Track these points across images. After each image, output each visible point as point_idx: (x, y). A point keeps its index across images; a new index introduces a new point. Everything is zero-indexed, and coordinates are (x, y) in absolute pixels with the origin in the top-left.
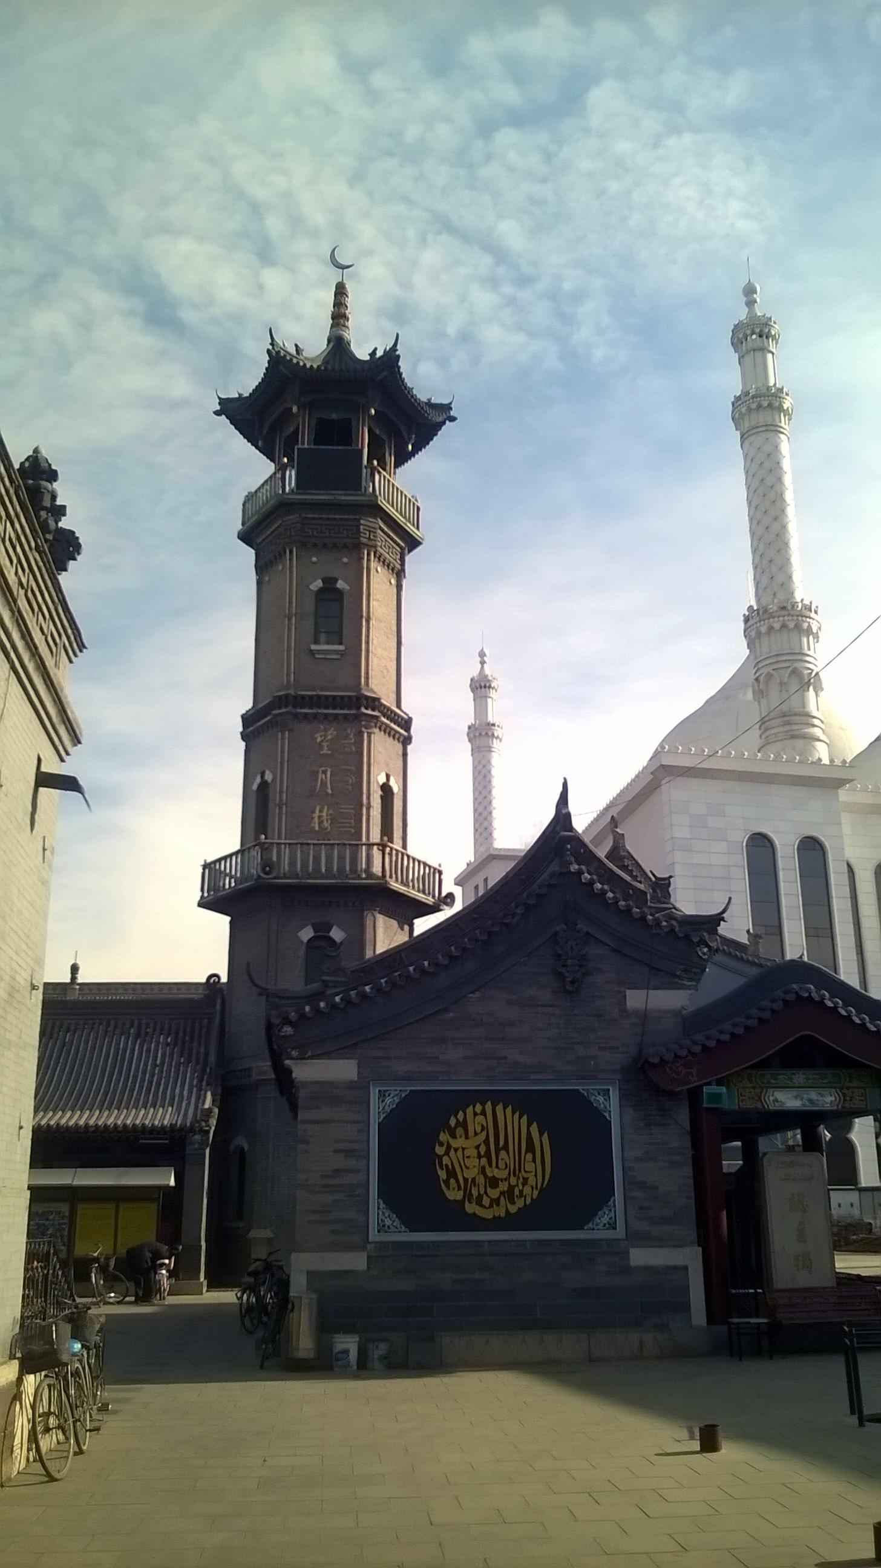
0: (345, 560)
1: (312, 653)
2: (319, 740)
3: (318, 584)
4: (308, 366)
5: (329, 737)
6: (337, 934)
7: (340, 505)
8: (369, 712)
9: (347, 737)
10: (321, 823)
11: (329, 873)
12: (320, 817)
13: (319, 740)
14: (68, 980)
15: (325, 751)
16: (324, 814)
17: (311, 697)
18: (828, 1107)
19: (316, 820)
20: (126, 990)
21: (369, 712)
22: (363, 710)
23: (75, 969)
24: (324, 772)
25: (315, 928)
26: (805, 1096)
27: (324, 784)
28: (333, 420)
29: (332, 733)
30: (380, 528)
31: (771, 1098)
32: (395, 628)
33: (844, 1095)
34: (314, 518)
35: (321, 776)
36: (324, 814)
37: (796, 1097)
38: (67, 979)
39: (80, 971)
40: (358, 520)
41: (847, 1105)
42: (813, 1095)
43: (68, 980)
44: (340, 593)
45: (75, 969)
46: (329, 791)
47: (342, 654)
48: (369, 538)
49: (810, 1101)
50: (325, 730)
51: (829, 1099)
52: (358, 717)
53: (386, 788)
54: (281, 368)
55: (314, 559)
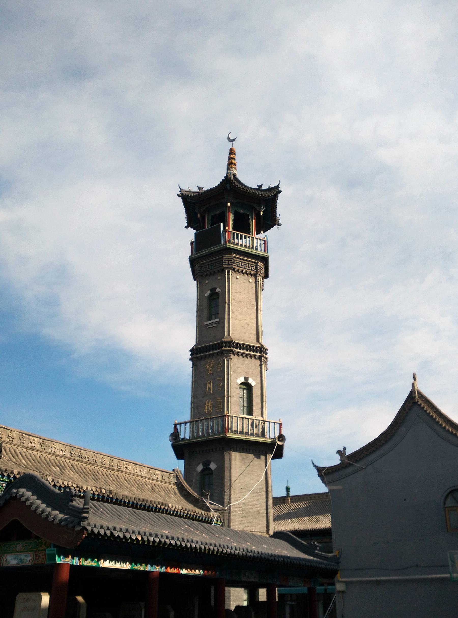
0: (219, 278)
1: (206, 326)
2: (207, 367)
3: (209, 292)
4: (195, 195)
5: (212, 365)
6: (213, 466)
7: (212, 253)
8: (228, 349)
9: (219, 364)
10: (208, 409)
11: (203, 435)
12: (208, 406)
13: (207, 367)
14: (286, 495)
15: (210, 372)
16: (210, 404)
17: (203, 347)
18: (28, 564)
19: (206, 408)
20: (311, 498)
21: (228, 349)
22: (224, 349)
23: (288, 489)
24: (210, 383)
25: (204, 465)
26: (19, 558)
27: (209, 388)
28: (218, 214)
29: (213, 362)
30: (235, 257)
31: (5, 560)
32: (254, 303)
33: (36, 555)
34: (205, 263)
35: (208, 385)
36: (210, 404)
37: (15, 559)
38: (284, 494)
39: (290, 490)
40: (222, 258)
41: (36, 562)
42: (22, 556)
43: (286, 495)
44: (217, 294)
45: (288, 489)
46: (212, 392)
47: (218, 323)
48: (228, 264)
49: (21, 560)
50: (210, 362)
51: (29, 558)
52: (222, 352)
53: (247, 386)
54: (188, 200)
55: (207, 282)
